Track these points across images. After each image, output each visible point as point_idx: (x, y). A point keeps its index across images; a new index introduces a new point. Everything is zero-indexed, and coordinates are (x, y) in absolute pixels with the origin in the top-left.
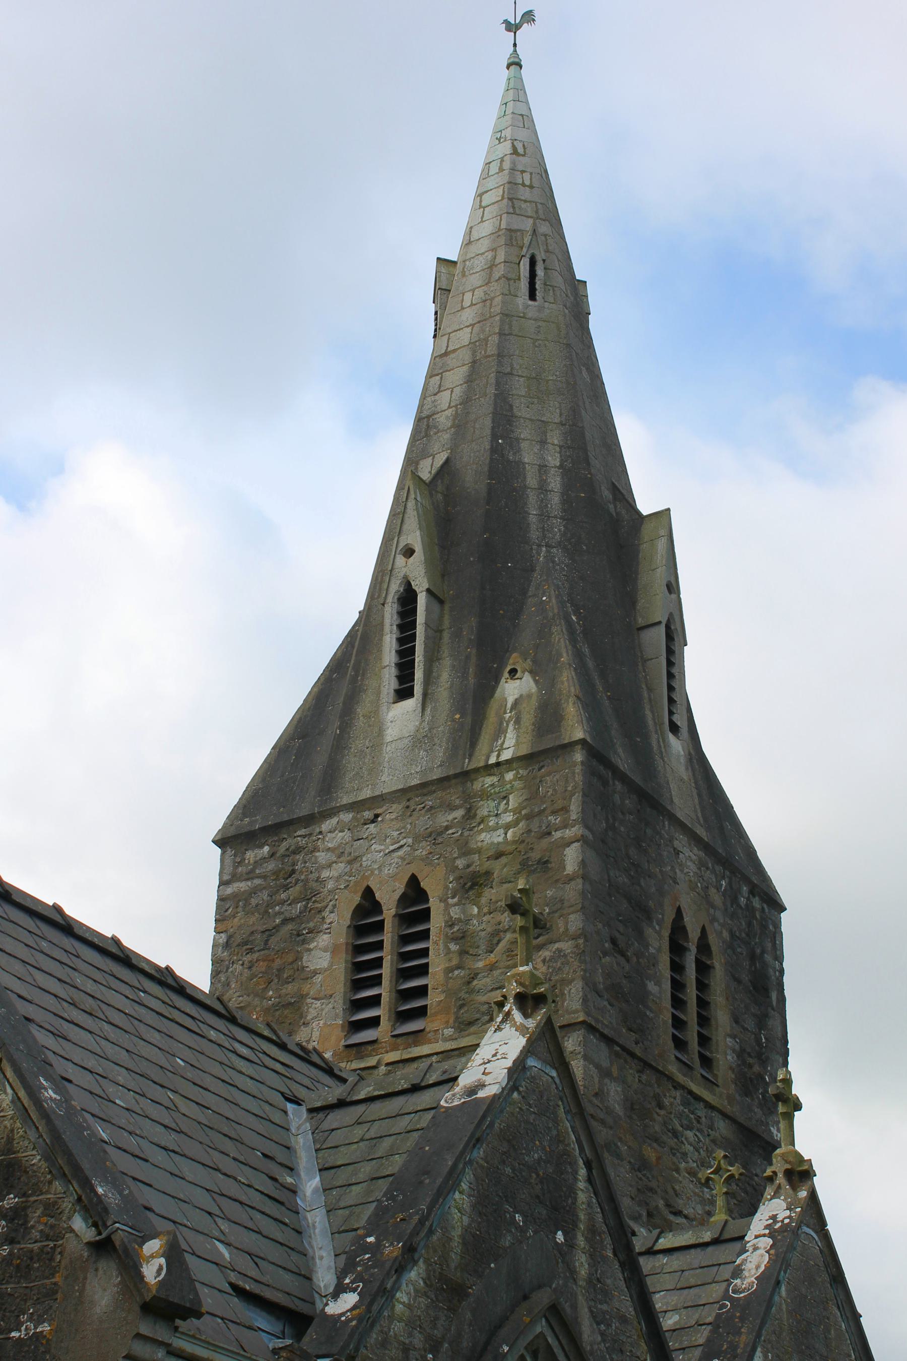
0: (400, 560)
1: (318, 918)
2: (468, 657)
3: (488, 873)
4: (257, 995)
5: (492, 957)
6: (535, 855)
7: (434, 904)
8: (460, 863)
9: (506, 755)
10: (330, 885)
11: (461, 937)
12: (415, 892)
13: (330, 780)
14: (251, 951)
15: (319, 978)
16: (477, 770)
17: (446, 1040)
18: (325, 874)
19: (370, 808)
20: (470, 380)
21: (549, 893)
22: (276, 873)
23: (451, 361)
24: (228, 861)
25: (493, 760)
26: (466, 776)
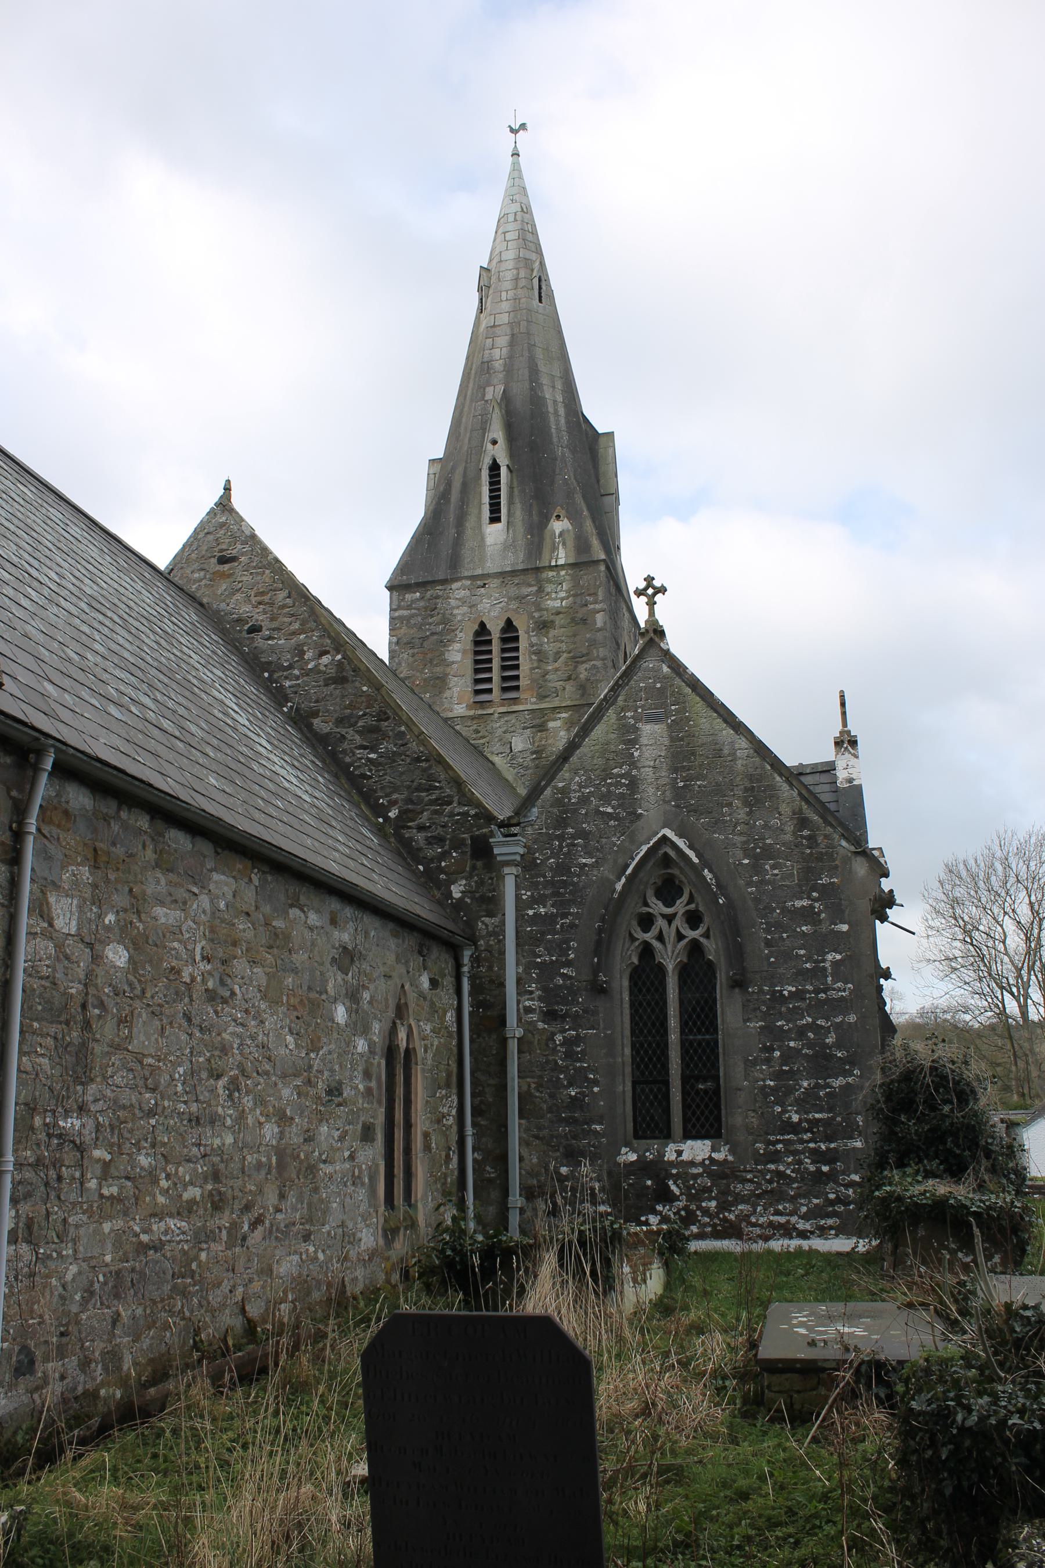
0: (490, 446)
1: (452, 634)
2: (531, 505)
3: (552, 622)
4: (418, 671)
5: (556, 665)
6: (579, 616)
7: (521, 633)
8: (536, 615)
9: (561, 562)
10: (459, 618)
11: (538, 653)
12: (509, 626)
13: (455, 562)
14: (413, 647)
15: (455, 666)
16: (544, 567)
17: (532, 704)
18: (456, 612)
19: (481, 580)
20: (512, 344)
21: (588, 636)
22: (426, 608)
23: (498, 331)
24: (395, 598)
25: (553, 563)
26: (538, 570)
